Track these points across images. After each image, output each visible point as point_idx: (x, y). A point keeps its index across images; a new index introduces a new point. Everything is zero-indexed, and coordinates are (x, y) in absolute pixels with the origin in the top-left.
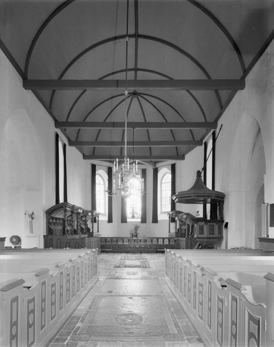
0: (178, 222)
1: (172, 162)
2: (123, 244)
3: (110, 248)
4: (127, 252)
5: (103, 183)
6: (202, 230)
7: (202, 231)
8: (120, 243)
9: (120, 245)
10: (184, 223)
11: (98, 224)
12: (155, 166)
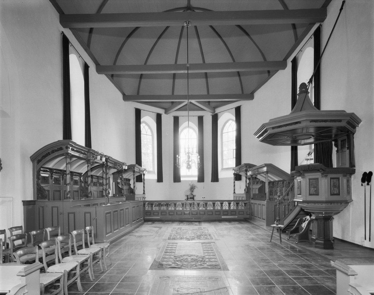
2: (175, 210)
3: (158, 215)
4: (181, 221)
5: (151, 134)
7: (314, 188)
8: (171, 208)
9: (171, 211)
11: (144, 183)
12: (215, 112)
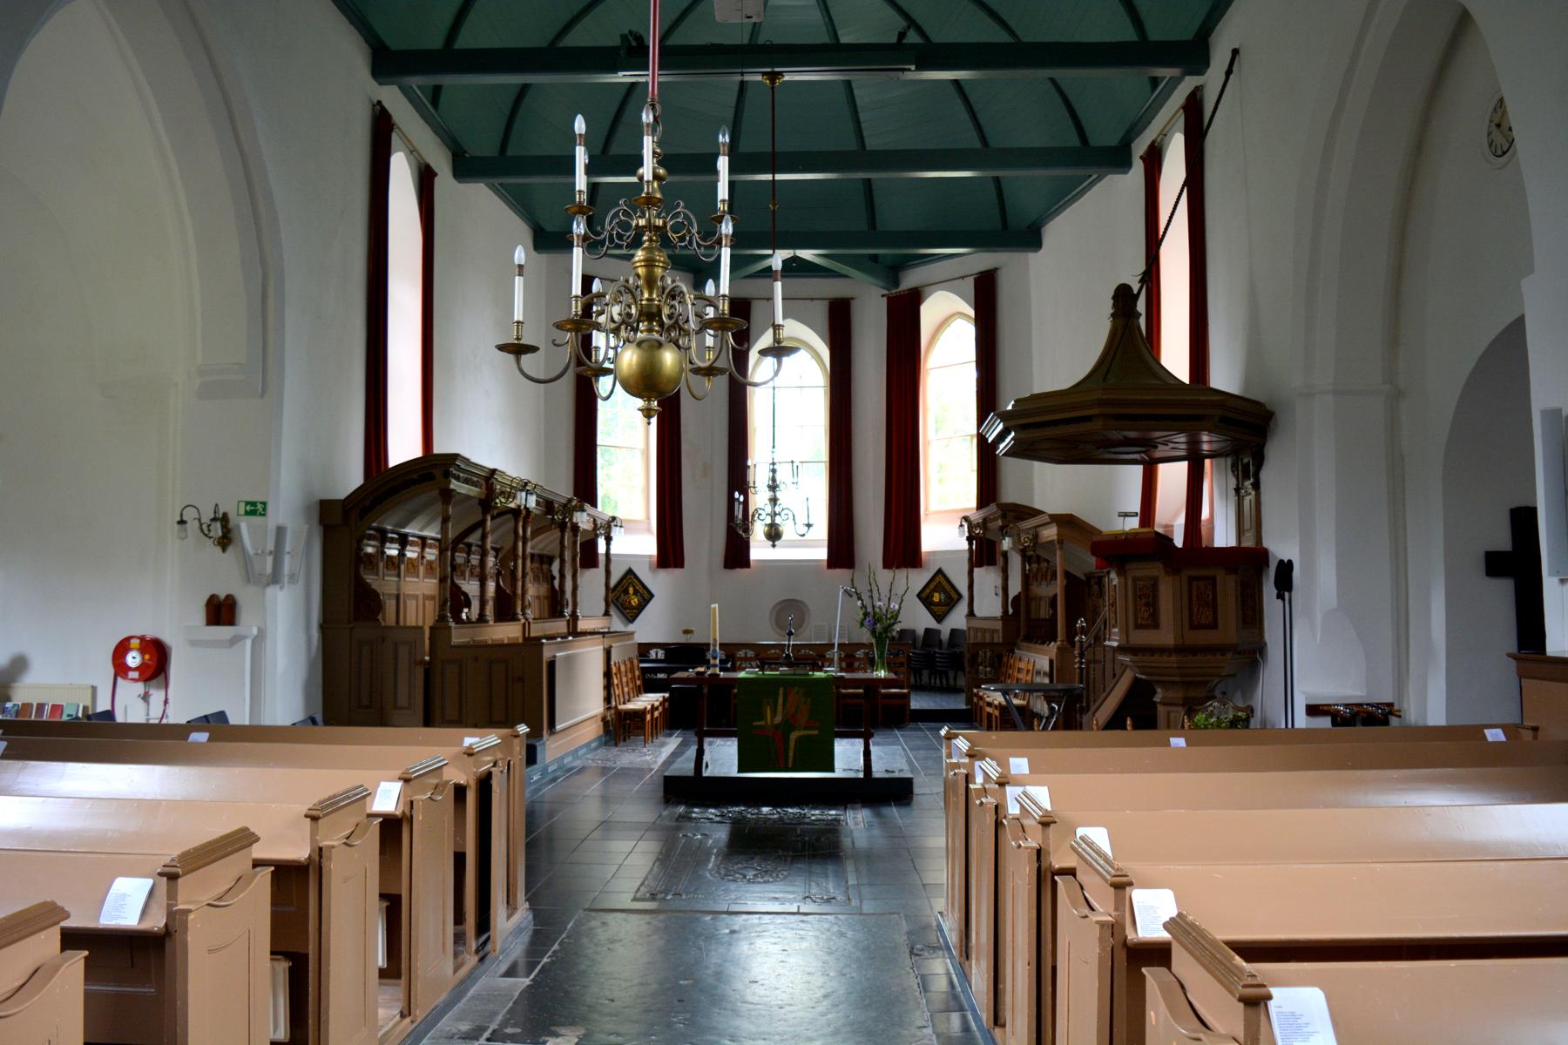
0: (1015, 562)
1: (982, 260)
6: (1147, 605)
10: (1044, 565)
